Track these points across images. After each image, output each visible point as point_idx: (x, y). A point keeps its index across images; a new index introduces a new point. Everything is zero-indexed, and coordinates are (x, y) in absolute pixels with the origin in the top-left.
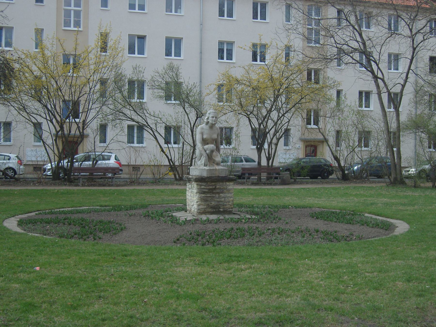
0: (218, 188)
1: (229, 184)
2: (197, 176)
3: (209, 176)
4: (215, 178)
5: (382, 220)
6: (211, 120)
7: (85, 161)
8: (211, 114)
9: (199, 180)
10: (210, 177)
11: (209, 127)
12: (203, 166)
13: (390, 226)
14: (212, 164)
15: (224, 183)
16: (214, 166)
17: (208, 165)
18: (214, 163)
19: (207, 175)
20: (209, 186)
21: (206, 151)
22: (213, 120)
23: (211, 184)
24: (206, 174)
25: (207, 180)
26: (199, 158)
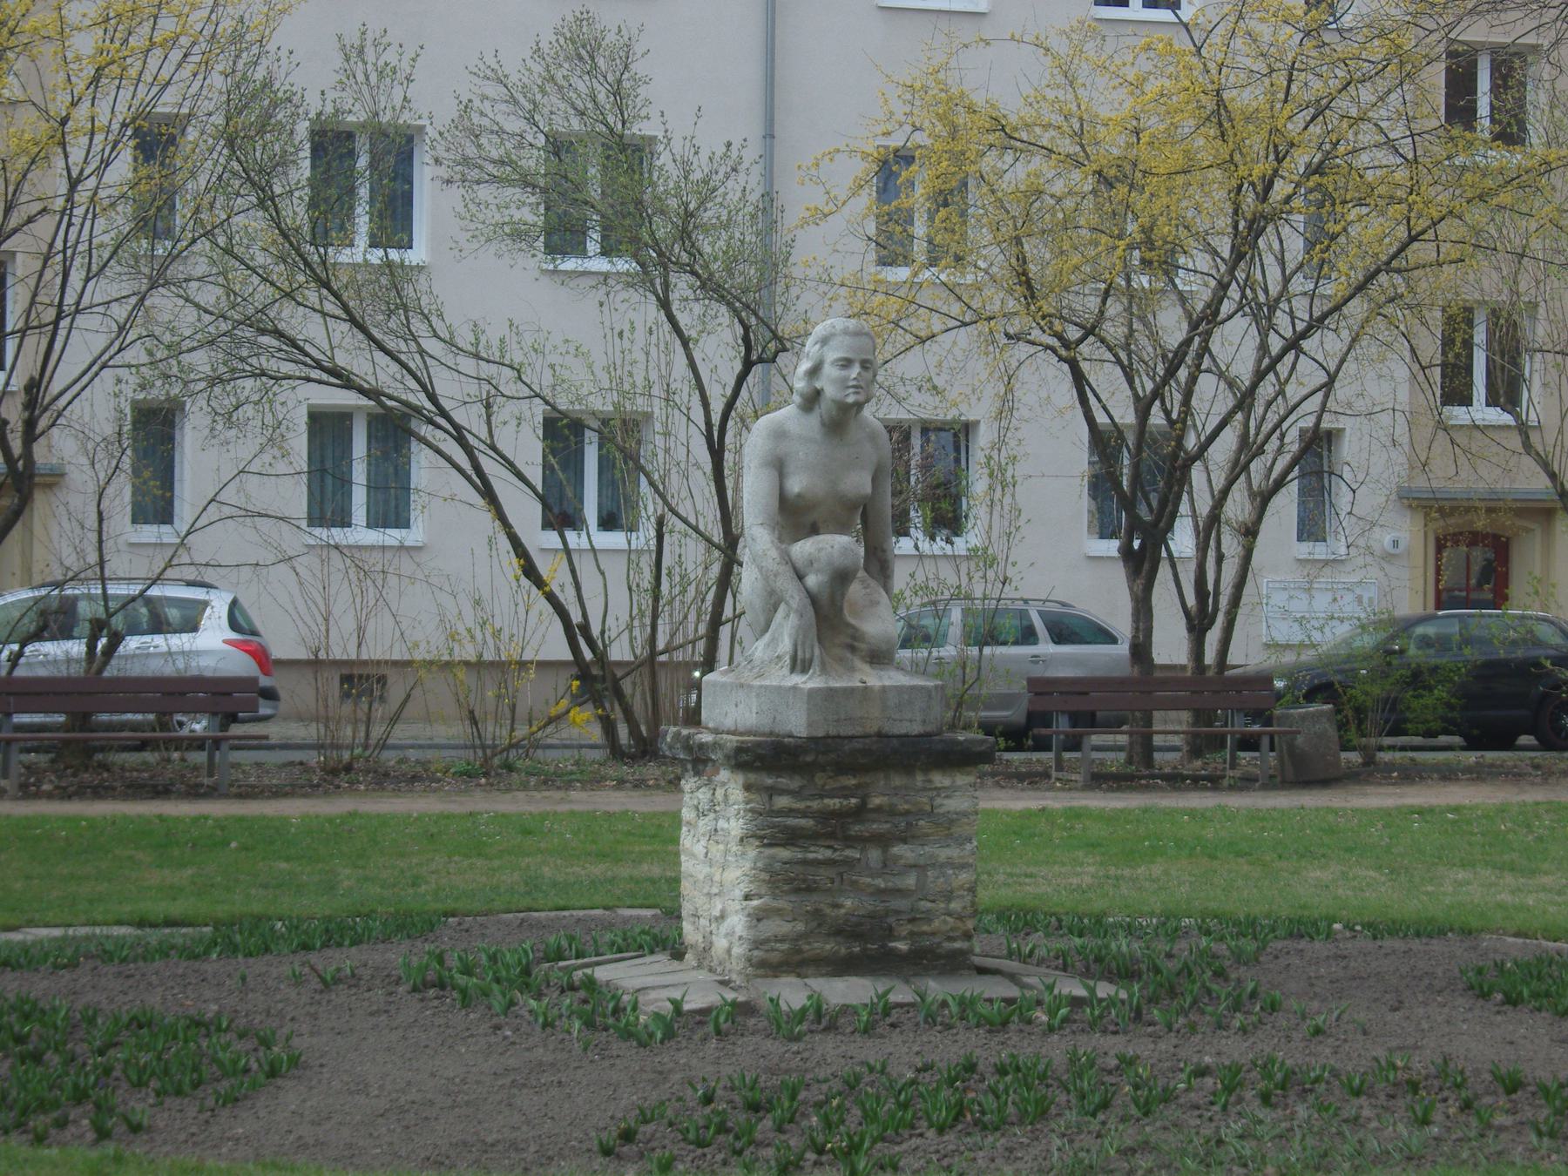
0: (879, 809)
3: (821, 734)
4: (857, 745)
9: (760, 758)
10: (827, 737)
12: (786, 671)
16: (852, 669)
17: (816, 662)
18: (853, 649)
19: (810, 725)
20: (822, 797)
22: (846, 379)
23: (831, 784)
25: (809, 758)
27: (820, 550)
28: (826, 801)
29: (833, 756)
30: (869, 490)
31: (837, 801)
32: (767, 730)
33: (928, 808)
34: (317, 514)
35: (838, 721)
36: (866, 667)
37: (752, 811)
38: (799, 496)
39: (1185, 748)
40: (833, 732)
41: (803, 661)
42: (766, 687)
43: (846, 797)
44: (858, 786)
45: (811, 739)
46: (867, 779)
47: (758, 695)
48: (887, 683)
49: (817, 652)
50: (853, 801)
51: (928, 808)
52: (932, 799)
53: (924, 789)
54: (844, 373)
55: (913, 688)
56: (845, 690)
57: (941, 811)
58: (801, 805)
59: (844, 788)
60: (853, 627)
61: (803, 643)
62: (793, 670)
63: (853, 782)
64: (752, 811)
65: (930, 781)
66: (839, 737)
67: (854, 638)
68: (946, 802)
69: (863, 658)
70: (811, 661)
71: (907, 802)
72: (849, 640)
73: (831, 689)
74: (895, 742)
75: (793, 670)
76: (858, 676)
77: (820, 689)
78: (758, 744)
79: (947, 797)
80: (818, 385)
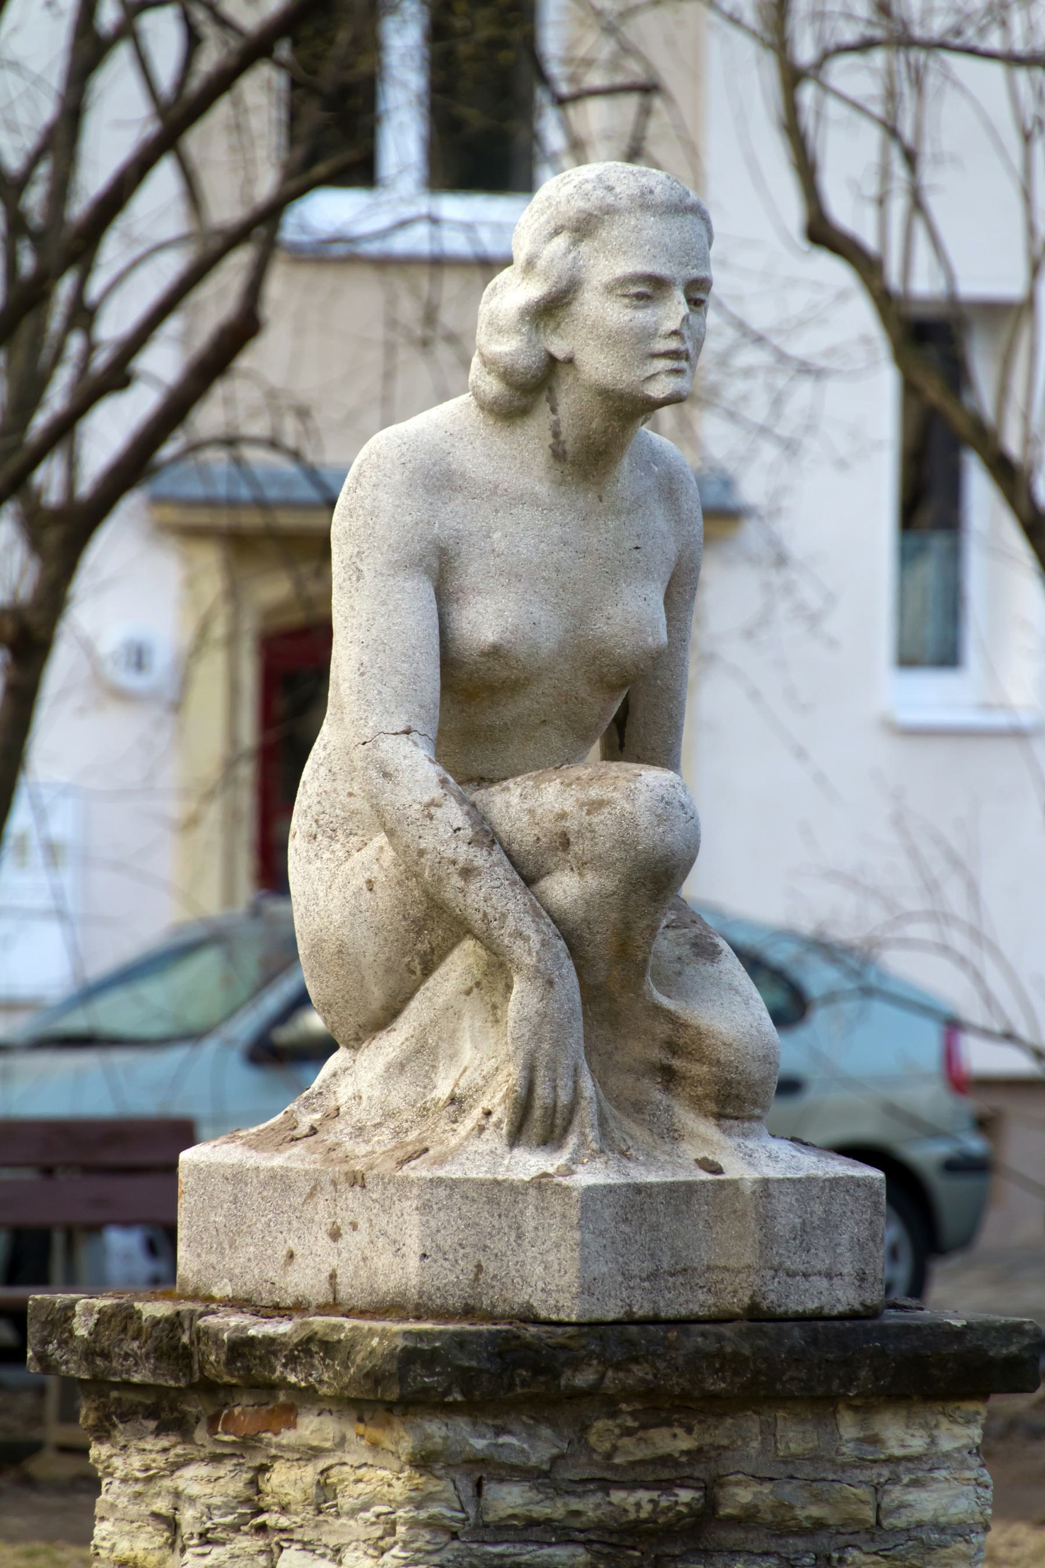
0: (747, 1519)
1: (917, 1444)
2: (442, 1314)
3: (612, 1311)
4: (697, 1340)
5: (455, 1334)
6: (613, 339)
7: (234, 1386)
8: (612, 233)
9: (466, 1379)
10: (630, 1320)
11: (558, 454)
12: (494, 1140)
13: (600, 179)
14: (637, 1108)
15: (848, 1428)
16: (673, 1135)
17: (587, 1113)
18: (669, 1077)
19: (587, 1289)
20: (605, 1485)
21: (530, 880)
22: (647, 334)
23: (632, 1450)
24: (570, 1279)
25: (584, 1378)
26: (377, 996)
27: (595, 806)
28: (618, 1496)
29: (639, 1371)
30: (664, 638)
31: (643, 1496)
32: (455, 1302)
33: (869, 1514)
34: (930, 633)
35: (653, 1276)
36: (707, 1128)
37: (432, 1524)
38: (495, 652)
39: (421, 1301)
40: (642, 1309)
41: (551, 1111)
42: (453, 1185)
43: (665, 1486)
44: (696, 1455)
45: (590, 1326)
46: (719, 1434)
47: (425, 1208)
48: (773, 1172)
49: (588, 1085)
50: (685, 1495)
51: (869, 1514)
52: (877, 1489)
53: (861, 1463)
54: (644, 316)
55: (835, 1183)
56: (672, 1188)
57: (899, 1521)
58: (555, 1509)
59: (666, 1460)
60: (671, 1018)
61: (552, 1066)
62: (516, 1136)
63: (685, 1443)
64: (432, 1524)
65: (875, 1440)
66: (655, 1320)
67: (672, 1047)
68: (913, 1496)
69: (697, 1104)
70: (572, 1109)
71: (817, 1498)
72: (657, 1055)
73: (638, 1189)
74: (796, 1333)
75: (516, 1136)
76: (691, 1152)
77: (610, 1189)
78: (460, 1341)
79: (916, 1483)
80: (559, 347)
